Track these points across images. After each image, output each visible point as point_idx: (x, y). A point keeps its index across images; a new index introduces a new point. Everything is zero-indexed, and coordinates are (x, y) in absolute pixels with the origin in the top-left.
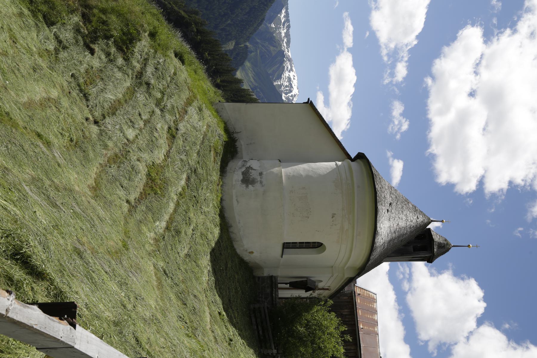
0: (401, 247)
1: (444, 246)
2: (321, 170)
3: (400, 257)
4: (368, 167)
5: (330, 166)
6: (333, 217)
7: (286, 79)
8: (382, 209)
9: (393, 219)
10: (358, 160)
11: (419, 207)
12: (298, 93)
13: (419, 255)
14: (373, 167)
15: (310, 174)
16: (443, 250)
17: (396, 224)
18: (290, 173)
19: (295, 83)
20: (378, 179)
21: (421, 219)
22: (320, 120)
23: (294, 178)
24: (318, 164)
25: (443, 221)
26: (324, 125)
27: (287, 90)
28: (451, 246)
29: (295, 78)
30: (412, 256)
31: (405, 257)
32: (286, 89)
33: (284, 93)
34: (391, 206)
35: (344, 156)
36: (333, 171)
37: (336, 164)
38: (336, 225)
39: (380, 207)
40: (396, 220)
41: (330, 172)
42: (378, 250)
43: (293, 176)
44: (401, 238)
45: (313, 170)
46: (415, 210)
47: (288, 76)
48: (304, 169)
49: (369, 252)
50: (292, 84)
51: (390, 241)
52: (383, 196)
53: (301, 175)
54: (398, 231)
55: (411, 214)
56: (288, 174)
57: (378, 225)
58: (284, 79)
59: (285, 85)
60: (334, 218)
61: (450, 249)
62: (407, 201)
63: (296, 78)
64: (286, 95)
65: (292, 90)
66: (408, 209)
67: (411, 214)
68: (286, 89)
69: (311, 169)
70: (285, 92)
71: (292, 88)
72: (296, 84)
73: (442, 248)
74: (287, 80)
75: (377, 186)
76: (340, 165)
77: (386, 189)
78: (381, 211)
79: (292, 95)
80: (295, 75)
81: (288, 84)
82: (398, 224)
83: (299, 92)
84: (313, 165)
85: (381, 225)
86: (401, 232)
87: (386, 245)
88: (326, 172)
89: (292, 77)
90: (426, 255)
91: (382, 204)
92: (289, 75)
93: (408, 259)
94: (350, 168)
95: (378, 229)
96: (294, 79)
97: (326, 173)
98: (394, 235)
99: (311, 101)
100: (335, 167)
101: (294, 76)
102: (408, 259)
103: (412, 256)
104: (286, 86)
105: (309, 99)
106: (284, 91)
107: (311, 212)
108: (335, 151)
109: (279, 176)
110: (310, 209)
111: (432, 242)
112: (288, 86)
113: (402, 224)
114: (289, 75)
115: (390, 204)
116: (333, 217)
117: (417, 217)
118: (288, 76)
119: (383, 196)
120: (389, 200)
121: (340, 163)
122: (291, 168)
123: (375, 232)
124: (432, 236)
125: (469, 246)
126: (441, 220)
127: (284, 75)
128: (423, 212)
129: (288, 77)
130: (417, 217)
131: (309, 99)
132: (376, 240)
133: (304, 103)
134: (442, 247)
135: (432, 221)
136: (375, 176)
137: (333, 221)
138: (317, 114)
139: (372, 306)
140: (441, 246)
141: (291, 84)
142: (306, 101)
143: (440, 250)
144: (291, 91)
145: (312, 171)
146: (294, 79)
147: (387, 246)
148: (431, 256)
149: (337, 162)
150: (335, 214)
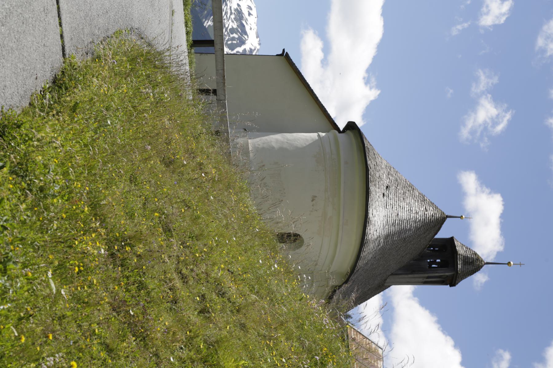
0: (412, 262)
1: (472, 262)
2: (298, 141)
3: (410, 276)
4: (360, 140)
5: (311, 137)
6: (313, 201)
7: (231, 13)
8: (376, 192)
9: (392, 206)
10: (348, 131)
11: (428, 197)
12: (258, 47)
13: (437, 273)
14: (365, 138)
15: (285, 146)
16: (471, 268)
17: (395, 214)
18: (259, 145)
19: (251, 24)
20: (371, 153)
21: (431, 212)
22: (299, 78)
23: (261, 151)
24: (295, 135)
25: (462, 216)
26: (304, 85)
27: (233, 39)
28: (483, 263)
29: (251, 12)
30: (426, 275)
31: (416, 275)
32: (231, 36)
33: (227, 44)
34: (388, 189)
35: (330, 126)
36: (314, 143)
37: (319, 135)
38: (316, 211)
39: (372, 188)
40: (395, 208)
41: (310, 144)
42: (371, 246)
43: (263, 148)
44: (403, 236)
45: (288, 142)
46: (423, 199)
47: (236, 7)
48: (277, 141)
49: (359, 246)
50: (244, 26)
51: (387, 236)
52: (377, 175)
53: (273, 148)
54: (399, 224)
55: (416, 204)
56: (257, 146)
57: (370, 211)
58: (226, 13)
59: (230, 27)
60: (314, 202)
61: (482, 267)
62: (412, 188)
63: (254, 12)
64: (232, 50)
65: (246, 40)
66: (413, 196)
67: (416, 204)
68: (231, 36)
69: (286, 141)
70: (229, 42)
71: (246, 33)
72: (254, 27)
73: (470, 265)
74: (233, 16)
75: (369, 162)
76: (323, 137)
77: (382, 168)
78: (374, 193)
79: (245, 50)
80: (253, 6)
81: (235, 26)
82: (398, 214)
83: (260, 44)
84: (289, 136)
85: (374, 211)
86: (402, 226)
87: (382, 240)
88: (305, 144)
89: (245, 11)
90: (447, 274)
91: (375, 185)
92: (238, 5)
93: (421, 280)
94: (336, 140)
95: (370, 215)
96: (250, 14)
97: (305, 145)
98: (393, 228)
99: (287, 53)
100: (317, 138)
101: (250, 8)
102: (421, 280)
103: (426, 275)
104: (233, 31)
105: (284, 50)
106: (228, 41)
107: (285, 193)
108: (317, 119)
109: (245, 150)
110: (284, 189)
111: (455, 255)
112: (237, 29)
113: (404, 215)
114: (238, 5)
115: (387, 187)
116: (313, 201)
117: (426, 209)
118: (236, 7)
119: (377, 175)
120: (386, 182)
121: (323, 134)
122: (260, 138)
123: (366, 220)
124: (455, 247)
125: (509, 263)
126: (460, 216)
127: (226, 5)
128: (435, 203)
129: (236, 10)
130: (426, 209)
131: (284, 50)
132: (367, 230)
133: (277, 55)
134: (470, 263)
135: (447, 217)
136: (367, 150)
137: (313, 206)
138: (294, 70)
139: (376, 364)
140: (467, 262)
141: (242, 26)
142: (281, 52)
143: (467, 267)
144: (242, 42)
145: (287, 143)
146: (250, 14)
147: (384, 242)
148: (454, 275)
149: (320, 133)
150: (316, 197)
